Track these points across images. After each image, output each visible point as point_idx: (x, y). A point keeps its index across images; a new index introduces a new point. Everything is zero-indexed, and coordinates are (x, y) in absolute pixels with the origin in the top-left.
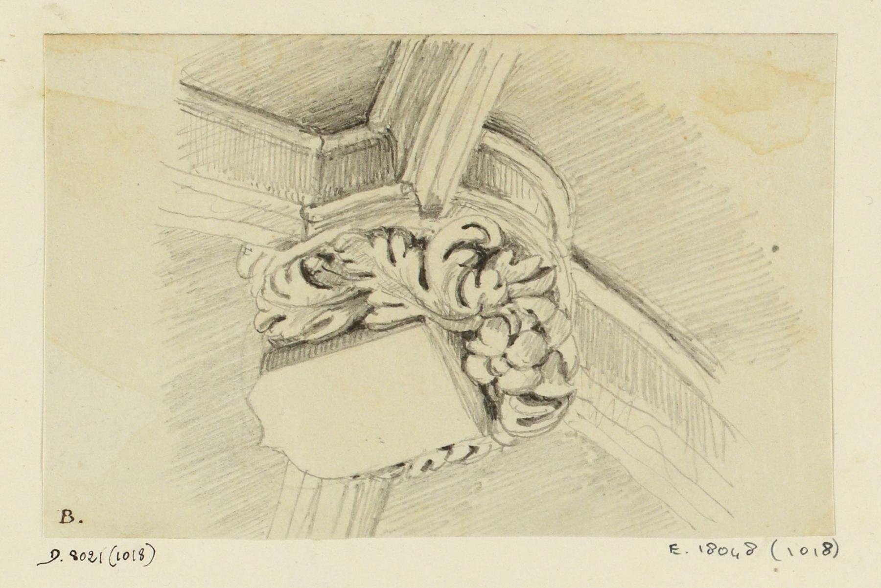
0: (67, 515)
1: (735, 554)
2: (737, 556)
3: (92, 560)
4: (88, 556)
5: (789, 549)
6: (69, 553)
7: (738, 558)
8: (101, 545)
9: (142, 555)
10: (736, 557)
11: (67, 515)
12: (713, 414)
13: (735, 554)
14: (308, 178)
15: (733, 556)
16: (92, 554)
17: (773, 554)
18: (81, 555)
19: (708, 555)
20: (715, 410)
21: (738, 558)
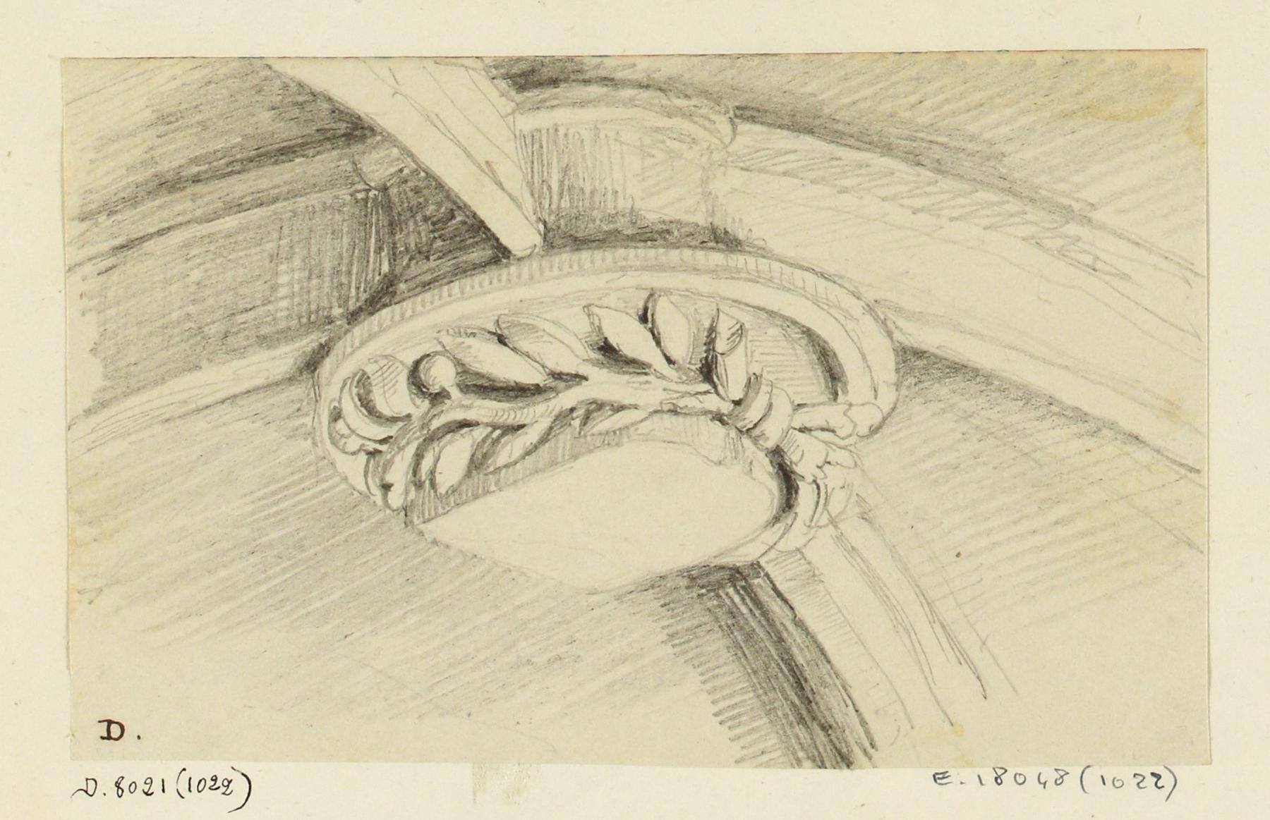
0: (112, 730)
1: (1042, 781)
2: (1045, 783)
3: (227, 793)
4: (210, 783)
5: (183, 798)
6: (933, 773)
7: (1044, 787)
8: (165, 770)
9: (118, 787)
10: (1042, 786)
11: (112, 730)
12: (512, 128)
13: (1042, 781)
14: (324, 486)
15: (1040, 783)
16: (216, 780)
17: (1081, 777)
18: (130, 785)
19: (1055, 786)
20: (510, 129)
21: (1044, 787)
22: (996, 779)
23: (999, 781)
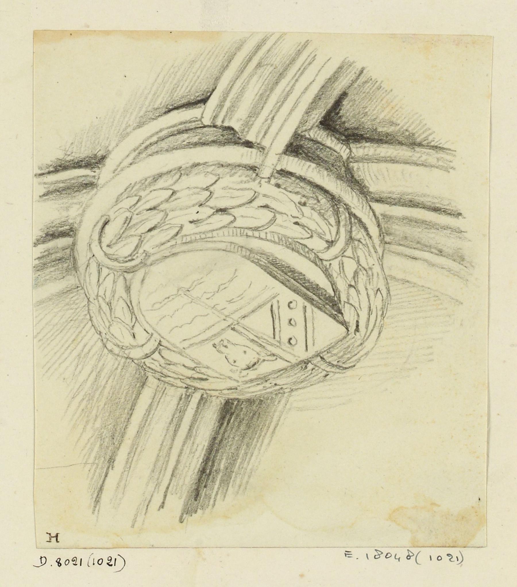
2: (399, 559)
7: (399, 561)
10: (398, 560)
21: (399, 561)
22: (407, 556)
23: (409, 558)
